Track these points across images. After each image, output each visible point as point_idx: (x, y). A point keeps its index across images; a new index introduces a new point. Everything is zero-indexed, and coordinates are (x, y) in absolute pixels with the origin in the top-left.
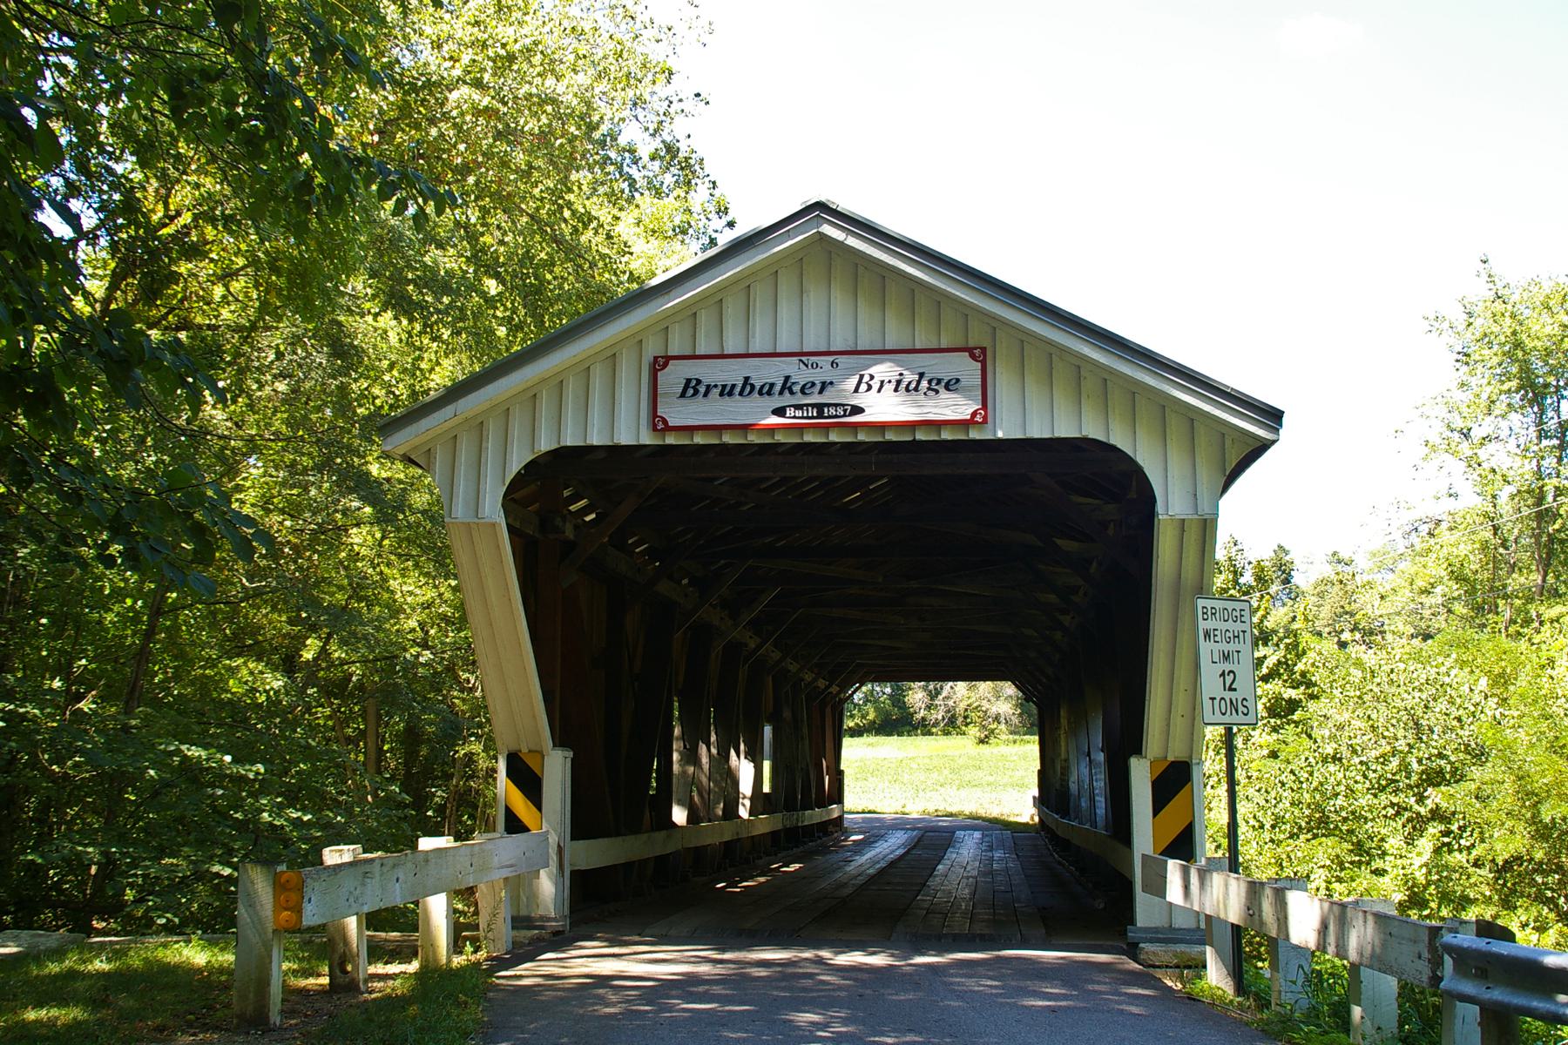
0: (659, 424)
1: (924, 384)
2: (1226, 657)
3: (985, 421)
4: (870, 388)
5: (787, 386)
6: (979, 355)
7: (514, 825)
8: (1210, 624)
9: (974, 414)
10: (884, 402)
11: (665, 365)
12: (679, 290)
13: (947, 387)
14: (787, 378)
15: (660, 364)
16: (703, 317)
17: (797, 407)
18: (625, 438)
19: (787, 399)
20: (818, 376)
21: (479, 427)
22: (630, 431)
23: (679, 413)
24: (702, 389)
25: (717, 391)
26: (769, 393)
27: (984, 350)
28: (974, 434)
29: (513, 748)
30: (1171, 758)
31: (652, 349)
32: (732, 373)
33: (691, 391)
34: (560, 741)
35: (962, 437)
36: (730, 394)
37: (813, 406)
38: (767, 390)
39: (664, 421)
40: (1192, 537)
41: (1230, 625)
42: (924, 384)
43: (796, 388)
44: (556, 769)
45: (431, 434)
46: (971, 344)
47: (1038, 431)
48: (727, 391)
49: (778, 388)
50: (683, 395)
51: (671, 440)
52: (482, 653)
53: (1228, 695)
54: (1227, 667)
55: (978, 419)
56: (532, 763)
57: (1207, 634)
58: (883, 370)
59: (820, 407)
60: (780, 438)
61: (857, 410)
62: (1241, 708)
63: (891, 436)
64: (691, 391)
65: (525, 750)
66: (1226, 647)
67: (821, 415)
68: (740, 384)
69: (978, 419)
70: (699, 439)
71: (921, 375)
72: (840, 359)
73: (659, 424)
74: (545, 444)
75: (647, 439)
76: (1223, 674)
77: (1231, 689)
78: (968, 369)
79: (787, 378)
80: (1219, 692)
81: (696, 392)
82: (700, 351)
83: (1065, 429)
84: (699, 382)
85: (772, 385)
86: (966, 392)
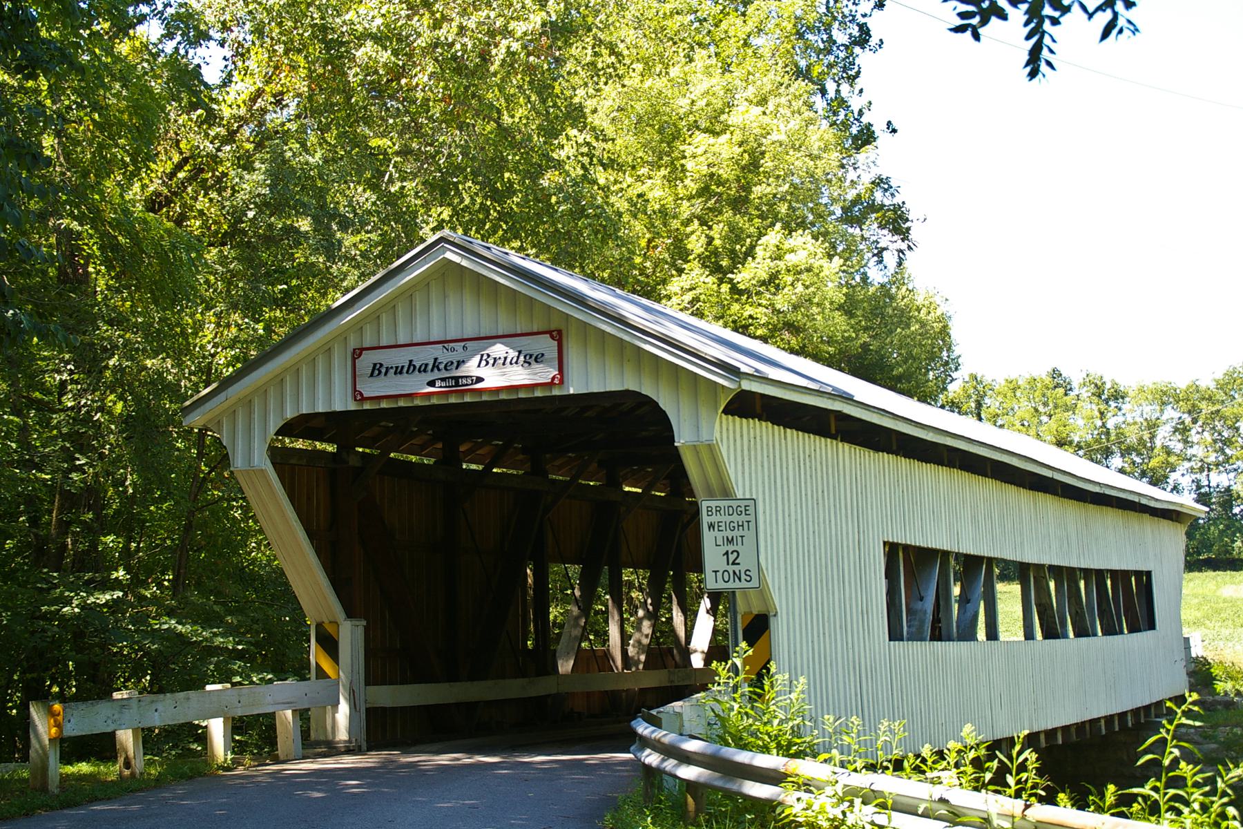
0: (358, 396)
1: (522, 358)
2: (730, 541)
3: (562, 382)
4: (487, 363)
5: (436, 366)
6: (558, 336)
7: (321, 674)
8: (714, 519)
9: (553, 378)
10: (498, 372)
11: (360, 355)
12: (359, 304)
13: (536, 361)
14: (436, 359)
15: (357, 353)
16: (384, 318)
17: (443, 380)
18: (338, 407)
19: (437, 375)
20: (454, 357)
21: (248, 403)
22: (341, 402)
23: (372, 388)
24: (383, 370)
25: (392, 371)
26: (425, 371)
27: (560, 332)
28: (556, 392)
29: (319, 620)
30: (755, 612)
31: (353, 343)
32: (400, 358)
33: (484, 363)
34: (350, 615)
35: (515, 397)
36: (401, 373)
37: (452, 378)
38: (423, 369)
39: (361, 394)
40: (705, 455)
41: (735, 518)
42: (522, 358)
43: (442, 366)
44: (350, 635)
45: (217, 411)
46: (553, 327)
47: (595, 388)
48: (399, 371)
49: (430, 367)
50: (372, 375)
51: (367, 406)
52: (279, 555)
53: (731, 568)
54: (731, 548)
55: (556, 381)
56: (330, 629)
57: (711, 526)
58: (498, 350)
59: (456, 379)
60: (435, 401)
61: (480, 380)
62: (743, 577)
63: (503, 396)
64: (484, 363)
65: (326, 621)
66: (730, 534)
67: (457, 385)
68: (406, 365)
69: (556, 381)
70: (384, 405)
71: (520, 352)
72: (469, 344)
73: (358, 396)
74: (290, 414)
75: (352, 406)
76: (727, 553)
77: (733, 563)
78: (547, 345)
79: (436, 359)
80: (721, 564)
81: (380, 372)
82: (384, 343)
83: (613, 385)
84: (381, 365)
85: (426, 365)
86: (548, 363)
